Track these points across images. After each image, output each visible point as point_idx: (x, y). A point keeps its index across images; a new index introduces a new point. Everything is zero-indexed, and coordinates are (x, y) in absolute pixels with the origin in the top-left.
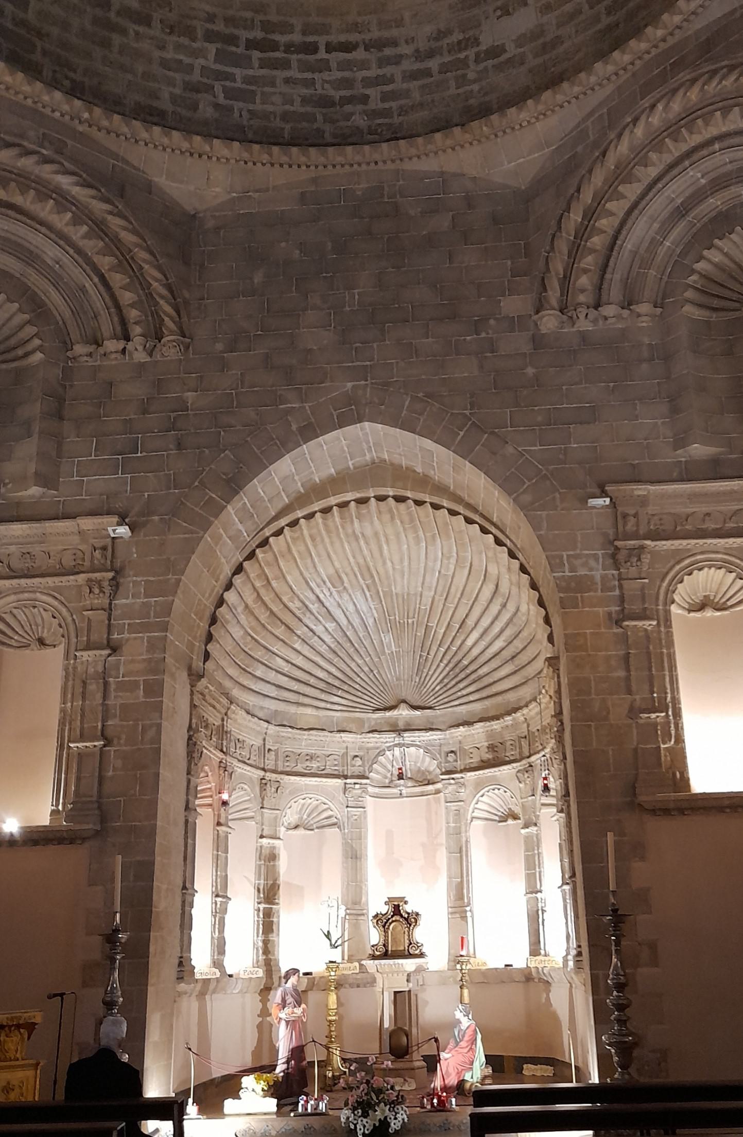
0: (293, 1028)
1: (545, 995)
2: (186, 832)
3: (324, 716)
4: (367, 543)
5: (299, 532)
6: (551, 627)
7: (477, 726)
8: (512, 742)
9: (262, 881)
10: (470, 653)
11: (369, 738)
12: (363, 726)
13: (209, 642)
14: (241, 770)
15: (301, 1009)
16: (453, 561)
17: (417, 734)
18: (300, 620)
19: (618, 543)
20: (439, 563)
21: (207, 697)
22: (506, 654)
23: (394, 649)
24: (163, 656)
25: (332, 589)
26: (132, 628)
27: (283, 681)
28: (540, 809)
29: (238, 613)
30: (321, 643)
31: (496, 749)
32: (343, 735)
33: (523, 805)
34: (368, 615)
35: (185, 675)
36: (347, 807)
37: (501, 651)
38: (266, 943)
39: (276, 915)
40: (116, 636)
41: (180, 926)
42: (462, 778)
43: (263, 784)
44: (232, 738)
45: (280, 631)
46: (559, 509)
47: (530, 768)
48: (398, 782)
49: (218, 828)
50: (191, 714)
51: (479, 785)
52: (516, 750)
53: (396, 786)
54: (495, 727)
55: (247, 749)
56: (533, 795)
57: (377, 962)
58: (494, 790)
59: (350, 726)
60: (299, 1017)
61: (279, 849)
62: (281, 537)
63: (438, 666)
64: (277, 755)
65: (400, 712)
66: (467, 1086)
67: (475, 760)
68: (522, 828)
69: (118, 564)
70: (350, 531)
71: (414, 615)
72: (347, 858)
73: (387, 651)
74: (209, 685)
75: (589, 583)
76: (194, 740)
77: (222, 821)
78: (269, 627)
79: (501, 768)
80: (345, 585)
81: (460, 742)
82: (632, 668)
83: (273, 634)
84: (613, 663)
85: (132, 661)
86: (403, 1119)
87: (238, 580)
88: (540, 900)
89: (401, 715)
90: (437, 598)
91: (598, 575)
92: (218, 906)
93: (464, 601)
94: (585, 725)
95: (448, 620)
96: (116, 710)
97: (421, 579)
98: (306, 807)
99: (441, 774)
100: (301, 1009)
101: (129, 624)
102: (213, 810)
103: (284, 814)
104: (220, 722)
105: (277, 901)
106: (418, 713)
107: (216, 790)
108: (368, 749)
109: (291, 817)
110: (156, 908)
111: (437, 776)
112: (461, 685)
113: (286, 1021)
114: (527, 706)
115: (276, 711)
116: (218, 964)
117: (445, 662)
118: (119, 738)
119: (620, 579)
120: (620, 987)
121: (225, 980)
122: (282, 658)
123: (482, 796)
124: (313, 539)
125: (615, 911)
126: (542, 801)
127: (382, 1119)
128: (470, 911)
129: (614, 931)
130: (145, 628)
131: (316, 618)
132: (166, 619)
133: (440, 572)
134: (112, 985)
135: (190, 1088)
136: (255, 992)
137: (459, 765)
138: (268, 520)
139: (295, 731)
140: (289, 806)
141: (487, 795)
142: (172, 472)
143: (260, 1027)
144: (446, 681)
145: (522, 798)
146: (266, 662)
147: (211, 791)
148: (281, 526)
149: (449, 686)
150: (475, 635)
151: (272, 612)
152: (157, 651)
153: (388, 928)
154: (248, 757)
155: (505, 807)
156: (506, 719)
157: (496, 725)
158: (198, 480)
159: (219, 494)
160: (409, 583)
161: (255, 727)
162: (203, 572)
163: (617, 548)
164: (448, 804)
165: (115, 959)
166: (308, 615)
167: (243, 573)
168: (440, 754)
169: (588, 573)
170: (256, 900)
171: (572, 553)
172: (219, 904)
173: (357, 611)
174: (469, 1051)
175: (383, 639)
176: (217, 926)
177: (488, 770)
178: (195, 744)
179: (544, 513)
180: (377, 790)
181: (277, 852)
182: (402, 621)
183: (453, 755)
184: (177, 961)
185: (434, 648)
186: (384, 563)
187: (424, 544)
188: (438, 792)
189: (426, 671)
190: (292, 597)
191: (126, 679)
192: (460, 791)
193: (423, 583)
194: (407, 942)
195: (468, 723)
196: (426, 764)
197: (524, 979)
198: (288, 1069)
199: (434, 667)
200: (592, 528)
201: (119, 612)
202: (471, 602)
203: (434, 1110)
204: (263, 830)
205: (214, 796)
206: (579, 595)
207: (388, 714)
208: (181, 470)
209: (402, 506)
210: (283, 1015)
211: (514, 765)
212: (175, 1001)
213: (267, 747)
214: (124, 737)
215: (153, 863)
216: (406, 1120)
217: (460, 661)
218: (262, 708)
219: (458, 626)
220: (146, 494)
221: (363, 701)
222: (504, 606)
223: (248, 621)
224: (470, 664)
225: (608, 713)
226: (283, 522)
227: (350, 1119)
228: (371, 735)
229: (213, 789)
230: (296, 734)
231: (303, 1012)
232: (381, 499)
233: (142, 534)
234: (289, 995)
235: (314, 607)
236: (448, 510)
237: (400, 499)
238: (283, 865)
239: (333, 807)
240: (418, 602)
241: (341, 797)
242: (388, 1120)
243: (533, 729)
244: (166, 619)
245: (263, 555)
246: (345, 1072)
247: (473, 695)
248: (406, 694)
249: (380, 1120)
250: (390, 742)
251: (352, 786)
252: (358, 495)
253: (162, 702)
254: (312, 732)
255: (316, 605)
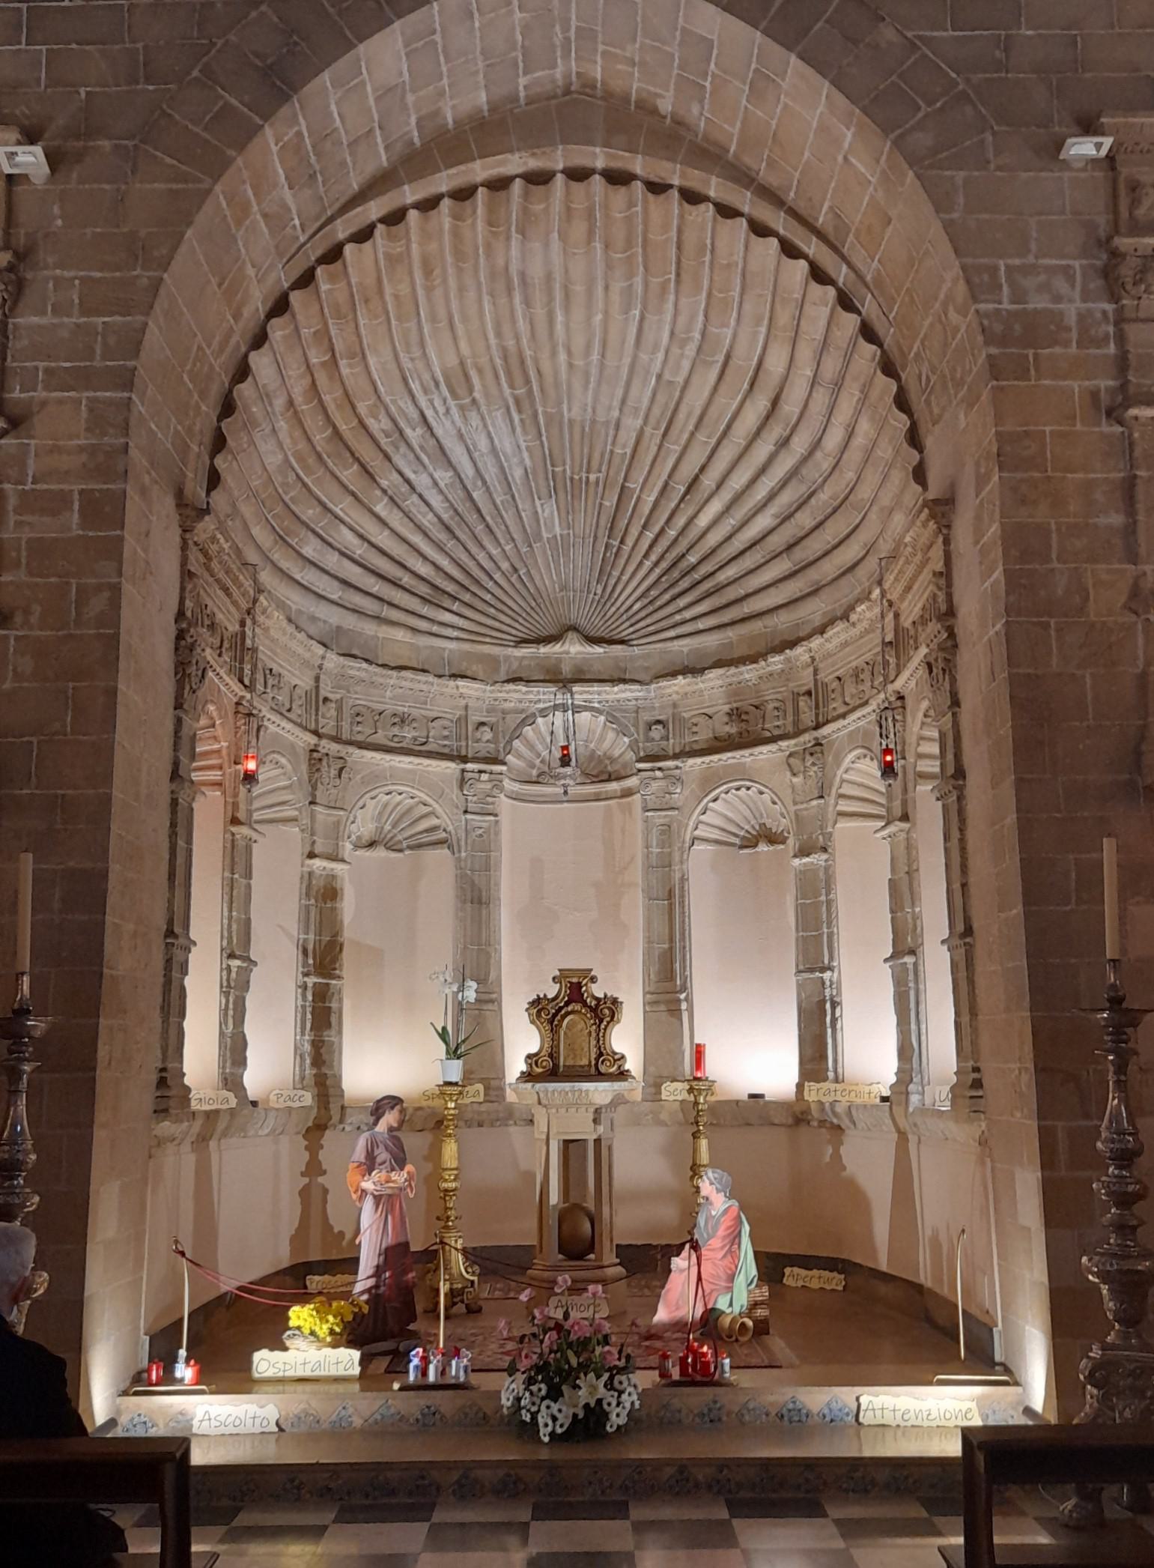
0: (390, 1210)
1: (830, 1150)
2: (173, 825)
3: (426, 647)
4: (527, 303)
5: (403, 242)
6: (921, 451)
7: (711, 675)
8: (777, 704)
9: (311, 936)
10: (703, 541)
11: (508, 692)
12: (497, 670)
13: (219, 451)
14: (277, 726)
15: (404, 1174)
16: (690, 350)
17: (596, 688)
18: (387, 457)
19: (1124, 243)
20: (660, 356)
21: (215, 565)
22: (777, 541)
23: (558, 530)
24: (122, 440)
25: (451, 403)
26: (55, 380)
27: (353, 573)
28: (835, 823)
29: (274, 413)
30: (424, 508)
31: (743, 717)
32: (460, 683)
33: (797, 815)
34: (515, 460)
35: (170, 501)
36: (466, 812)
37: (764, 537)
38: (318, 1045)
39: (336, 997)
40: (16, 394)
41: (162, 1008)
42: (677, 768)
43: (315, 759)
44: (260, 666)
45: (349, 474)
46: (992, 166)
47: (818, 748)
48: (562, 770)
49: (234, 829)
50: (183, 589)
51: (709, 783)
52: (785, 718)
53: (557, 777)
54: (747, 676)
55: (286, 690)
56: (822, 797)
57: (538, 1086)
58: (738, 789)
59: (474, 668)
60: (400, 1189)
61: (343, 879)
62: (367, 246)
63: (641, 563)
64: (339, 709)
65: (566, 647)
66: (726, 1321)
67: (704, 735)
68: (795, 856)
69: (21, 238)
70: (500, 262)
71: (601, 465)
72: (464, 902)
73: (545, 535)
74: (219, 536)
75: (1052, 327)
76: (189, 640)
77: (241, 815)
78: (330, 464)
79: (757, 750)
80: (477, 395)
81: (675, 705)
82: (1140, 507)
83: (337, 478)
84: (1098, 496)
85: (55, 450)
86: (633, 1403)
87: (278, 330)
88: (828, 983)
89: (568, 653)
90: (648, 430)
91: (1071, 311)
92: (233, 975)
93: (701, 437)
94: (1034, 624)
95: (664, 477)
96: (19, 550)
97: (619, 393)
98: (390, 808)
99: (637, 761)
100: (404, 1174)
101: (47, 370)
102: (224, 793)
103: (351, 819)
104: (237, 627)
105: (337, 972)
106: (598, 650)
107: (229, 755)
108: (504, 712)
109: (364, 825)
110: (111, 968)
111: (625, 766)
112: (682, 602)
113: (375, 1197)
114: (821, 630)
115: (339, 628)
116: (232, 1081)
117: (653, 557)
118: (27, 612)
119: (1120, 320)
120: (1125, 1158)
121: (245, 1112)
122: (352, 529)
123: (715, 800)
124: (428, 272)
125: (1116, 1002)
126: (839, 808)
127: (592, 1405)
128: (686, 999)
129: (1113, 1041)
130: (84, 378)
131: (418, 458)
132: (130, 364)
133: (659, 377)
134: (14, 1126)
135: (181, 1320)
136: (298, 1133)
137: (672, 745)
138: (343, 200)
139: (373, 668)
140: (360, 804)
141: (724, 800)
142: (140, 45)
143: (305, 1193)
144: (653, 593)
145: (795, 803)
146: (321, 532)
147: (221, 757)
148: (369, 222)
149: (658, 603)
150: (715, 507)
151: (336, 432)
152: (111, 431)
153: (560, 1025)
154: (288, 706)
155: (753, 822)
156: (771, 660)
157: (749, 673)
158: (199, 67)
159: (246, 98)
160: (596, 400)
161: (300, 650)
162: (209, 281)
163: (1115, 254)
164: (650, 814)
165: (20, 1073)
166: (403, 449)
167: (287, 316)
168: (635, 726)
169: (1051, 306)
170: (301, 969)
171: (1017, 262)
172: (234, 970)
173: (494, 450)
174: (725, 1256)
175: (540, 511)
176: (231, 1012)
177: (729, 755)
178: (191, 648)
179: (960, 176)
180: (516, 787)
181: (338, 887)
182: (576, 477)
183: (660, 727)
184: (154, 1077)
185: (634, 532)
186: (554, 354)
187: (637, 312)
188: (628, 793)
189: (616, 573)
190: (375, 405)
191: (38, 487)
192: (671, 789)
193: (623, 402)
194: (594, 1050)
195: (692, 669)
196: (606, 745)
197: (790, 1121)
198: (377, 1286)
199: (630, 569)
200: (1063, 213)
201: (26, 342)
202: (713, 441)
203: (688, 1381)
204: (314, 842)
205: (226, 765)
206: (1031, 352)
207: (544, 650)
208: (162, 43)
209: (620, 195)
210: (368, 1185)
211: (784, 744)
212: (150, 1157)
213: (323, 693)
214: (37, 609)
215: (104, 875)
216: (637, 1405)
217: (683, 556)
218: (313, 619)
219: (683, 489)
220: (82, 91)
221: (497, 625)
222: (784, 443)
223: (291, 437)
224: (700, 562)
225: (1087, 599)
226: (375, 209)
227: (523, 1403)
228: (511, 686)
229: (224, 752)
230: (376, 674)
231: (409, 1180)
232: (578, 175)
233: (75, 175)
234: (381, 1146)
235: (415, 435)
236: (717, 205)
237: (617, 178)
238: (348, 907)
239: (439, 810)
240: (610, 442)
241: (455, 794)
242: (605, 1406)
243: (827, 676)
244: (130, 364)
245: (328, 286)
246: (472, 1282)
247: (704, 619)
248: (578, 614)
249: (587, 1406)
250: (544, 702)
251: (476, 775)
252: (533, 164)
253: (121, 539)
254: (404, 673)
255: (419, 431)
